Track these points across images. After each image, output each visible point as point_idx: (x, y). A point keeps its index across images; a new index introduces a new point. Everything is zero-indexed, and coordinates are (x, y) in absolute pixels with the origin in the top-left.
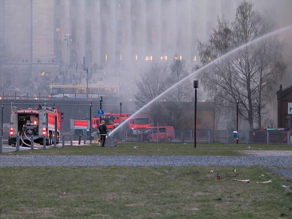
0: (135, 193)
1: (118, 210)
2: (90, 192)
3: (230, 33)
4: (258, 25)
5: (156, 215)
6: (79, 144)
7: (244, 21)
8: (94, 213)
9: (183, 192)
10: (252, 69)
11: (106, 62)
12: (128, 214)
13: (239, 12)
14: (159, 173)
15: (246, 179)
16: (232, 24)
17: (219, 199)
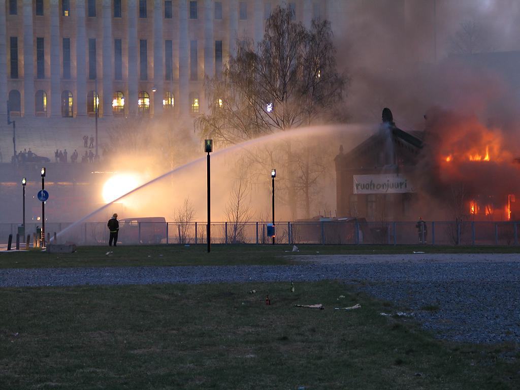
0: (138, 331)
1: (120, 360)
2: (60, 331)
3: (256, 59)
4: (302, 46)
5: (189, 367)
6: (9, 249)
7: (278, 40)
8: (82, 367)
9: (219, 328)
10: (293, 121)
11: (45, 110)
12: (140, 367)
13: (270, 25)
14: (166, 297)
15: (316, 304)
16: (259, 44)
17: (285, 338)
